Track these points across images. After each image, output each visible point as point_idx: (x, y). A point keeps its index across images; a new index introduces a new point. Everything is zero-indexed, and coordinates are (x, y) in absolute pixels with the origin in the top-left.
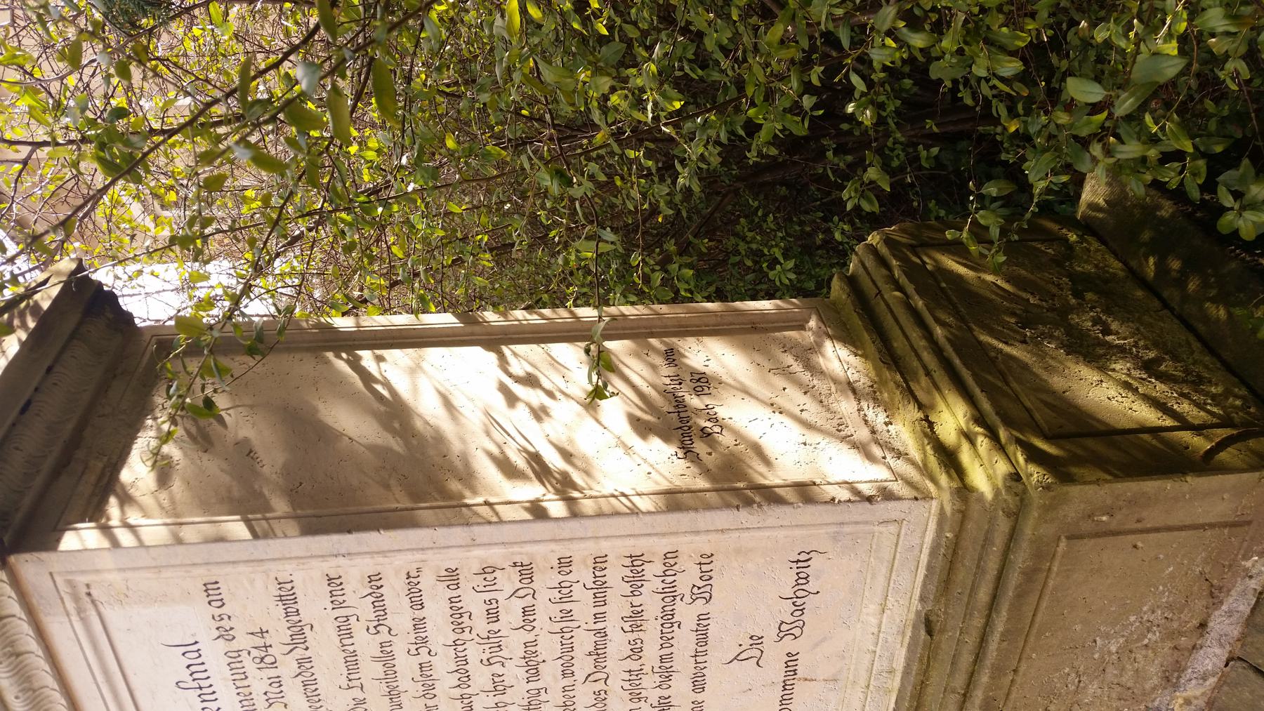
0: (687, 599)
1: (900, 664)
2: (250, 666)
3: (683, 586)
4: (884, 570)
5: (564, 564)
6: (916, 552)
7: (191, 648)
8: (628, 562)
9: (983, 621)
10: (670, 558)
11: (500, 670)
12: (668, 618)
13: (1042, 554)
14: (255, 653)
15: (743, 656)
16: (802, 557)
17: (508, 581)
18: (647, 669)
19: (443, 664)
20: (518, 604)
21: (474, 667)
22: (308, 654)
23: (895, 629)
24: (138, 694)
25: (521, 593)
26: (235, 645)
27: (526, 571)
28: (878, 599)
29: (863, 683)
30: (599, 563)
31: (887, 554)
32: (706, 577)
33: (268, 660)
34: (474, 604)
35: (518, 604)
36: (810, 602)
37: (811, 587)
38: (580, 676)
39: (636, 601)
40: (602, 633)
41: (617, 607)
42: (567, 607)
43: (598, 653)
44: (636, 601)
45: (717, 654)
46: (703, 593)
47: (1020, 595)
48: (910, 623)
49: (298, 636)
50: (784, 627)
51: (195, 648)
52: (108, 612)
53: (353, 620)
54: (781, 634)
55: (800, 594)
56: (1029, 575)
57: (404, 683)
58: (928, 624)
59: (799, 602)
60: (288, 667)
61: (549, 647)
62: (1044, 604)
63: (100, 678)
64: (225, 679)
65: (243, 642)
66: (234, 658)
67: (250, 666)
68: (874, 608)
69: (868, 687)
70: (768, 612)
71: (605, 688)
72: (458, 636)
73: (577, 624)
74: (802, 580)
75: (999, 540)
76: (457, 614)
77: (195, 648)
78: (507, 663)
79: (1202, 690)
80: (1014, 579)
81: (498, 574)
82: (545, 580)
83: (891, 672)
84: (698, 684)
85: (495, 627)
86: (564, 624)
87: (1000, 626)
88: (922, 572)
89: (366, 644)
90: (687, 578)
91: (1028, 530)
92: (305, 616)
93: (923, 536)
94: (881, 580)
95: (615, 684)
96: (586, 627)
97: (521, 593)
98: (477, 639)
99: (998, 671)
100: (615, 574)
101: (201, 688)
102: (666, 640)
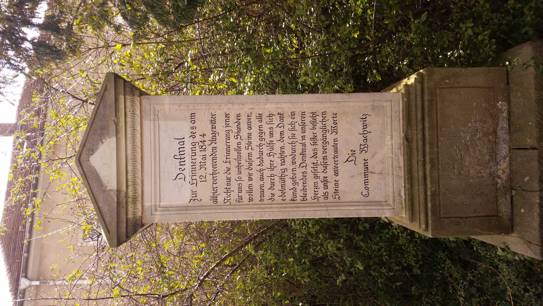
0: (330, 132)
1: (402, 164)
2: (198, 149)
3: (329, 128)
4: (389, 121)
5: (293, 114)
6: (398, 113)
7: (181, 141)
8: (311, 115)
9: (421, 126)
10: (324, 113)
11: (273, 159)
12: (324, 138)
13: (432, 94)
14: (201, 144)
15: (349, 160)
16: (364, 117)
17: (276, 120)
18: (319, 163)
19: (255, 154)
20: (279, 130)
21: (265, 156)
22: (216, 145)
23: (397, 147)
24: (161, 160)
25: (280, 125)
26: (195, 140)
27: (281, 116)
28: (390, 134)
29: (391, 172)
30: (303, 114)
31: (389, 115)
32: (335, 123)
33: (204, 147)
34: (266, 129)
35: (279, 130)
36: (369, 136)
37: (368, 129)
38: (298, 164)
39: (315, 131)
40: (304, 145)
41: (309, 134)
42: (294, 132)
43: (303, 154)
44: (315, 131)
45: (342, 158)
46: (335, 130)
47: (430, 111)
48: (402, 144)
49: (214, 140)
50: (362, 147)
51: (182, 140)
52: (161, 122)
53: (231, 131)
54: (361, 150)
55: (365, 132)
56: (431, 101)
57: (243, 162)
58: (407, 139)
59: (365, 136)
60: (209, 151)
61: (288, 151)
62: (439, 115)
63: (152, 149)
64: (189, 155)
65: (198, 139)
66: (194, 144)
67: (198, 149)
68: (389, 138)
69: (393, 174)
70: (356, 141)
71: (306, 171)
72: (261, 142)
73: (296, 140)
74: (365, 126)
75: (419, 93)
76: (261, 132)
77: (182, 140)
78: (275, 156)
79: (506, 164)
80: (426, 104)
81: (273, 117)
82: (288, 120)
83: (400, 167)
84: (336, 174)
85: (272, 139)
86: (293, 140)
87: (427, 125)
88: (401, 121)
89: (233, 142)
90: (329, 124)
91: (426, 85)
92: (217, 130)
93: (399, 107)
94: (389, 125)
95: (309, 169)
96: (299, 141)
97: (280, 125)
98: (266, 144)
99: (431, 144)
100: (308, 120)
101: (181, 159)
102: (325, 150)
